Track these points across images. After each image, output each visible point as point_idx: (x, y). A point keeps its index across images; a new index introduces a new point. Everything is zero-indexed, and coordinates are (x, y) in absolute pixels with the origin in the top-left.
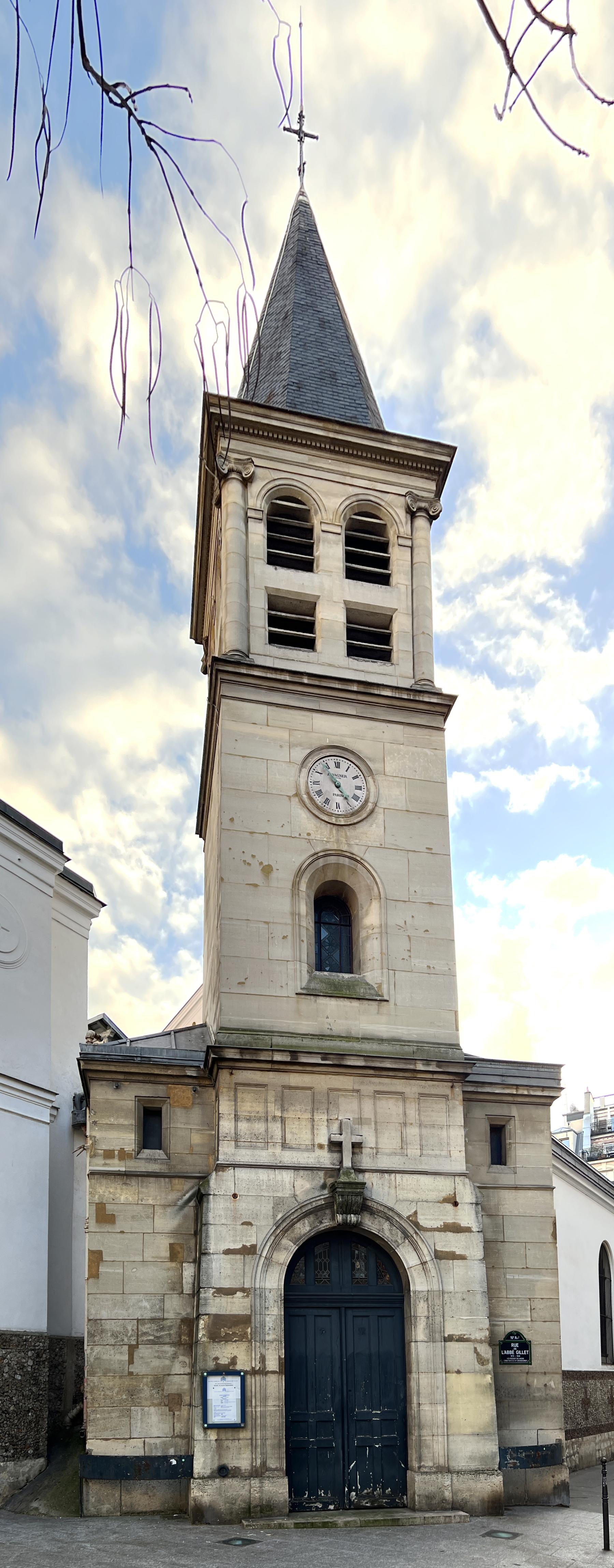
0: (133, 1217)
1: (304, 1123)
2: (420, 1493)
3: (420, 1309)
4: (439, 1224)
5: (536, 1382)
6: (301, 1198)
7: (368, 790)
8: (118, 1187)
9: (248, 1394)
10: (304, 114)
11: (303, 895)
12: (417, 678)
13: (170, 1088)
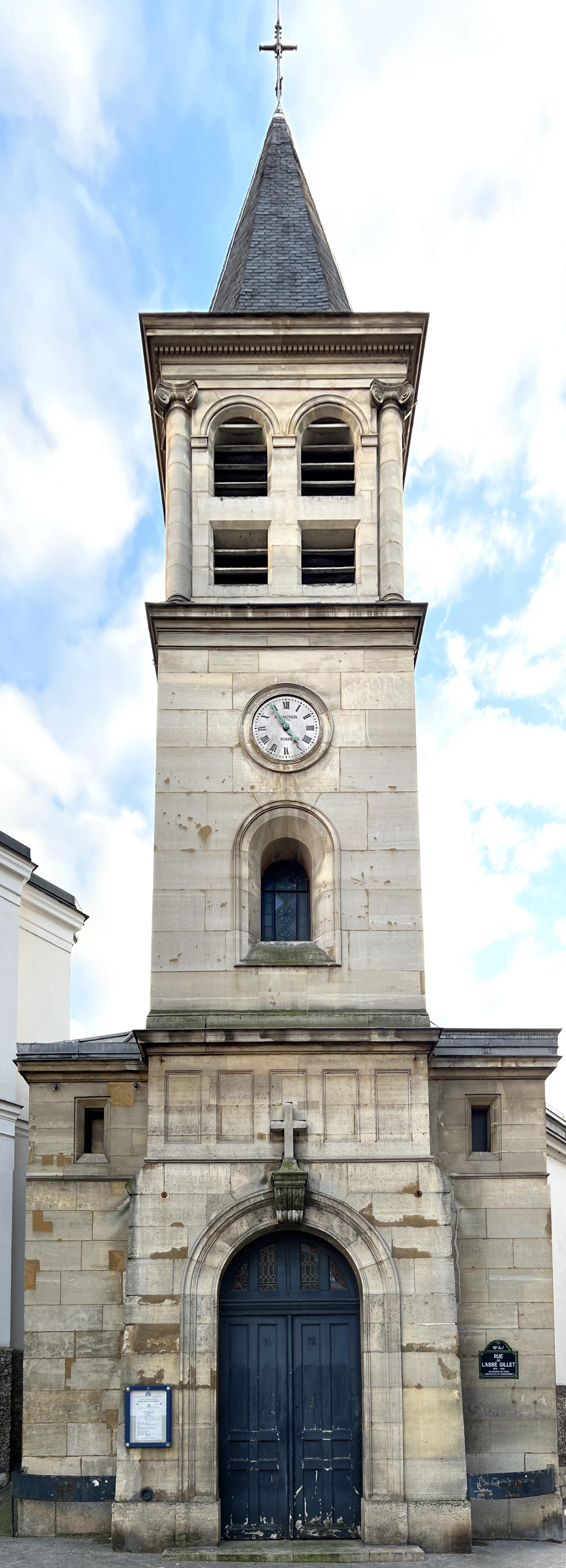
0: (71, 1224)
1: (243, 1111)
2: (370, 1524)
3: (374, 1316)
4: (398, 1217)
5: (524, 1399)
6: (239, 1195)
8: (56, 1193)
10: (281, 25)
12: (383, 595)
13: (111, 1086)
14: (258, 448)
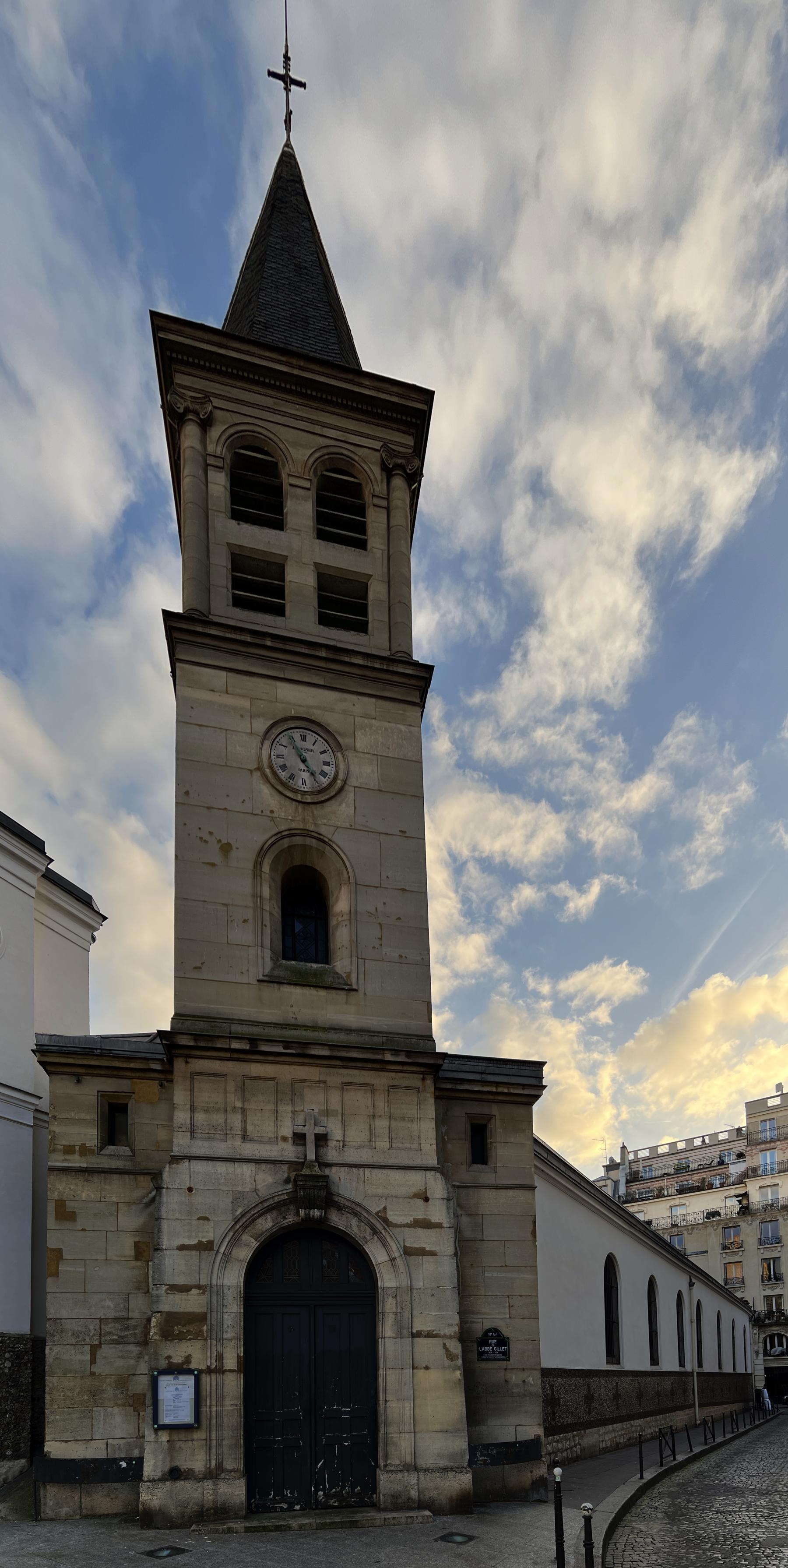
0: (95, 1215)
3: (388, 1306)
4: (409, 1220)
5: (514, 1378)
6: (263, 1192)
7: (337, 766)
9: (203, 1393)
12: (393, 652)
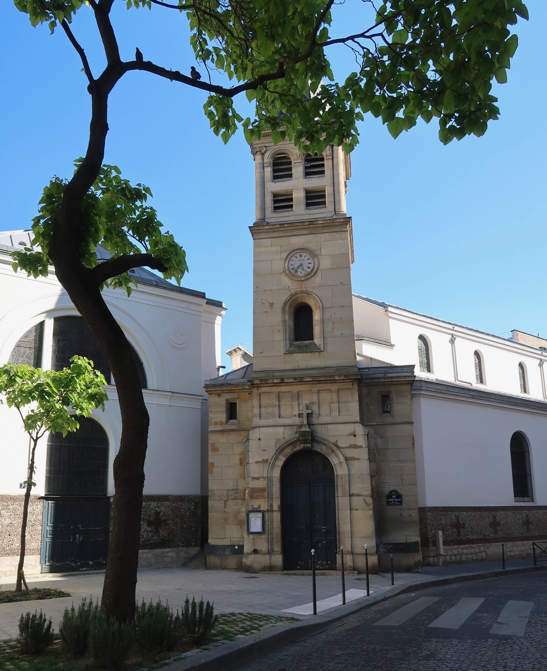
4: (348, 445)
6: (287, 438)
11: (287, 312)
14: (290, 160)
